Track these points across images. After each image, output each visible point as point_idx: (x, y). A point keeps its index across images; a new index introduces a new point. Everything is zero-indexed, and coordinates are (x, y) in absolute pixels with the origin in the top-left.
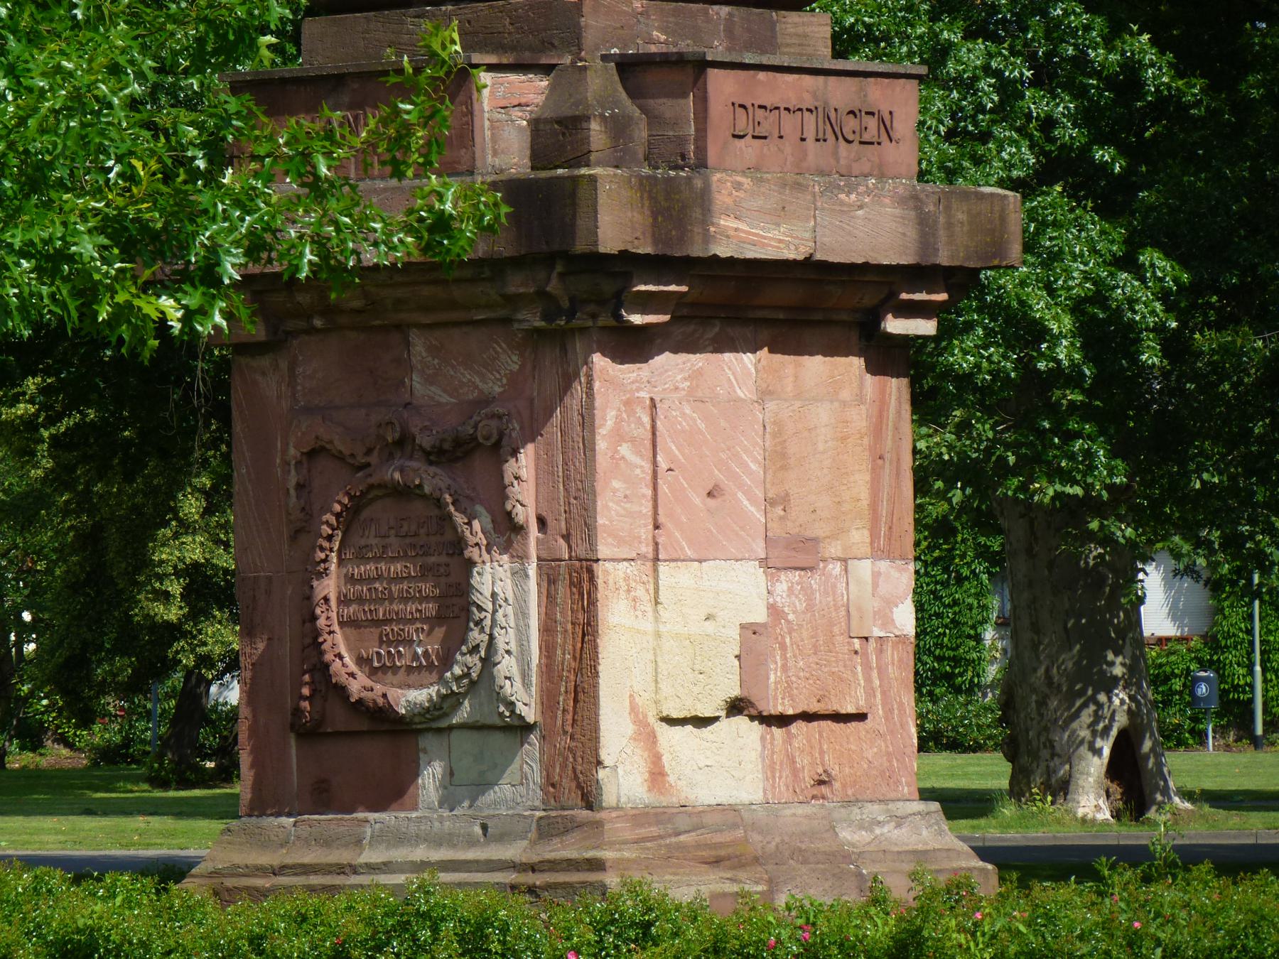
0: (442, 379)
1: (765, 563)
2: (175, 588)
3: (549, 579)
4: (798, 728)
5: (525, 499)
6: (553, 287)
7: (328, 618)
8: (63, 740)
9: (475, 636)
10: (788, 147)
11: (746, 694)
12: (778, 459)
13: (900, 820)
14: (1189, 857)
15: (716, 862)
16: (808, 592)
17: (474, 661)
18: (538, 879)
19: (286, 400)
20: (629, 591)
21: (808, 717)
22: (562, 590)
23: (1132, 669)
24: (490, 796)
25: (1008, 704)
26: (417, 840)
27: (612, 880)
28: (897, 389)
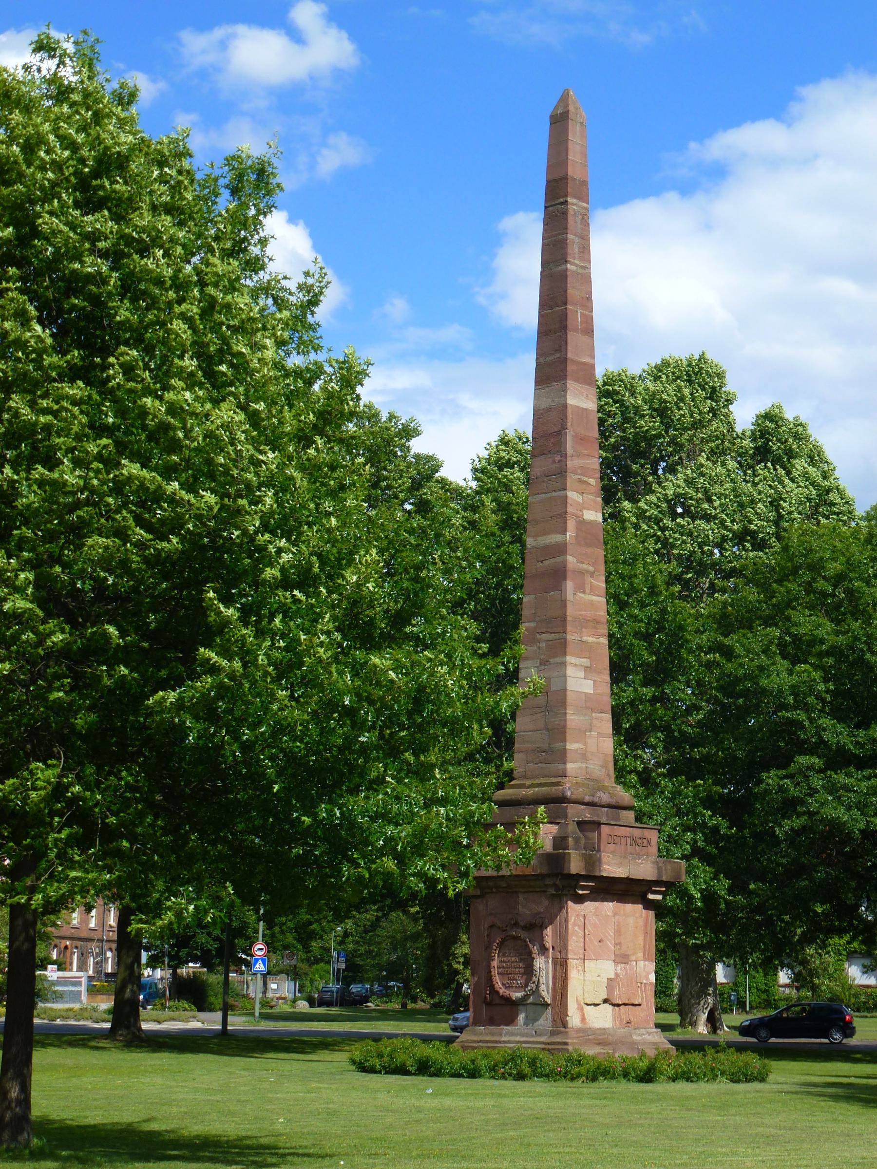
0: (527, 907)
1: (614, 961)
2: (462, 960)
3: (555, 963)
4: (622, 1007)
5: (549, 941)
6: (558, 882)
7: (495, 972)
8: (423, 1001)
9: (534, 979)
10: (623, 846)
12: (618, 932)
13: (649, 1034)
14: (730, 1045)
15: (599, 1044)
16: (626, 969)
17: (534, 986)
18: (550, 1047)
19: (485, 910)
21: (625, 1004)
22: (558, 967)
23: (714, 992)
24: (538, 1023)
25: (680, 1001)
26: (517, 1035)
27: (570, 1048)
28: (651, 914)
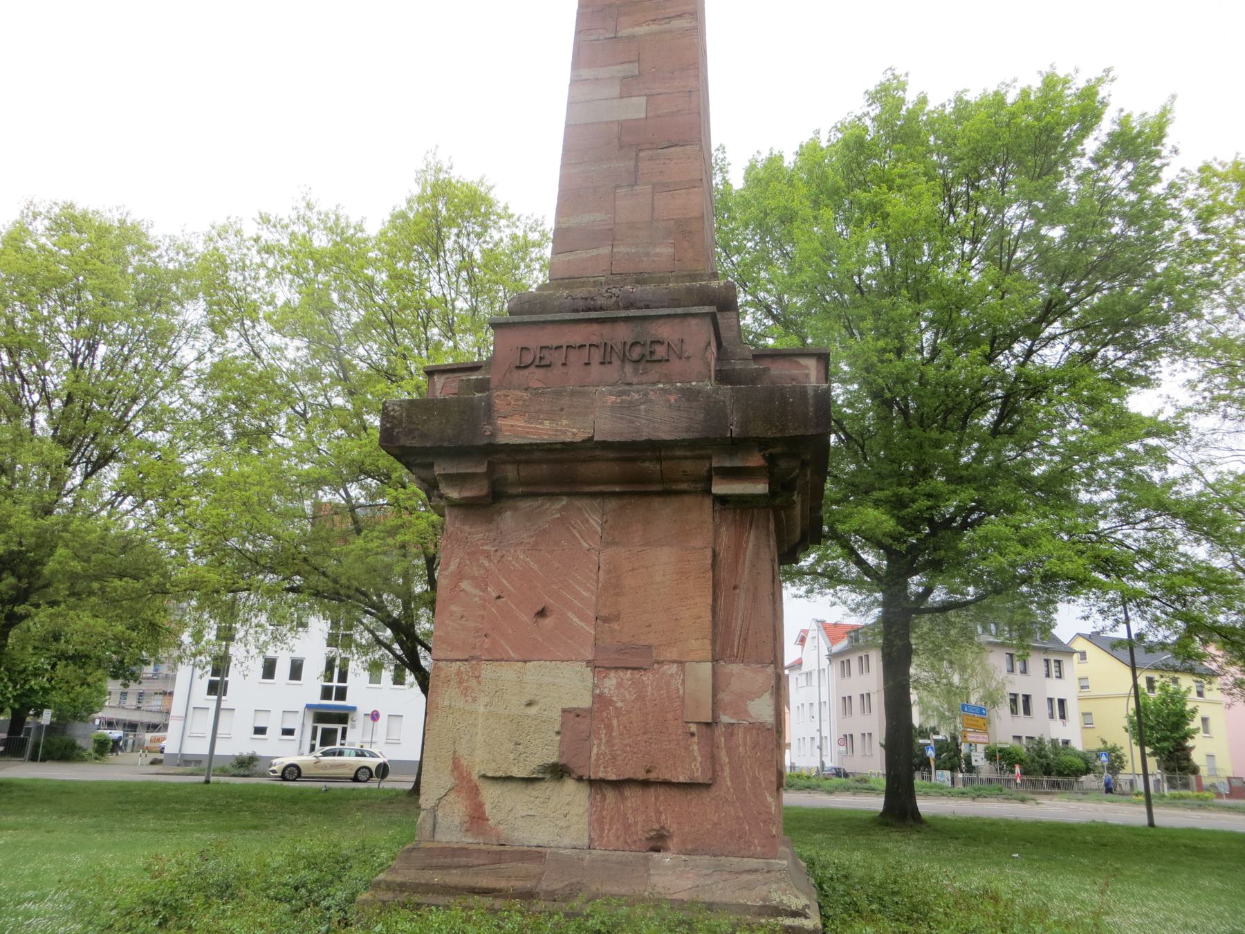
1: (593, 665)
11: (563, 761)
20: (461, 682)
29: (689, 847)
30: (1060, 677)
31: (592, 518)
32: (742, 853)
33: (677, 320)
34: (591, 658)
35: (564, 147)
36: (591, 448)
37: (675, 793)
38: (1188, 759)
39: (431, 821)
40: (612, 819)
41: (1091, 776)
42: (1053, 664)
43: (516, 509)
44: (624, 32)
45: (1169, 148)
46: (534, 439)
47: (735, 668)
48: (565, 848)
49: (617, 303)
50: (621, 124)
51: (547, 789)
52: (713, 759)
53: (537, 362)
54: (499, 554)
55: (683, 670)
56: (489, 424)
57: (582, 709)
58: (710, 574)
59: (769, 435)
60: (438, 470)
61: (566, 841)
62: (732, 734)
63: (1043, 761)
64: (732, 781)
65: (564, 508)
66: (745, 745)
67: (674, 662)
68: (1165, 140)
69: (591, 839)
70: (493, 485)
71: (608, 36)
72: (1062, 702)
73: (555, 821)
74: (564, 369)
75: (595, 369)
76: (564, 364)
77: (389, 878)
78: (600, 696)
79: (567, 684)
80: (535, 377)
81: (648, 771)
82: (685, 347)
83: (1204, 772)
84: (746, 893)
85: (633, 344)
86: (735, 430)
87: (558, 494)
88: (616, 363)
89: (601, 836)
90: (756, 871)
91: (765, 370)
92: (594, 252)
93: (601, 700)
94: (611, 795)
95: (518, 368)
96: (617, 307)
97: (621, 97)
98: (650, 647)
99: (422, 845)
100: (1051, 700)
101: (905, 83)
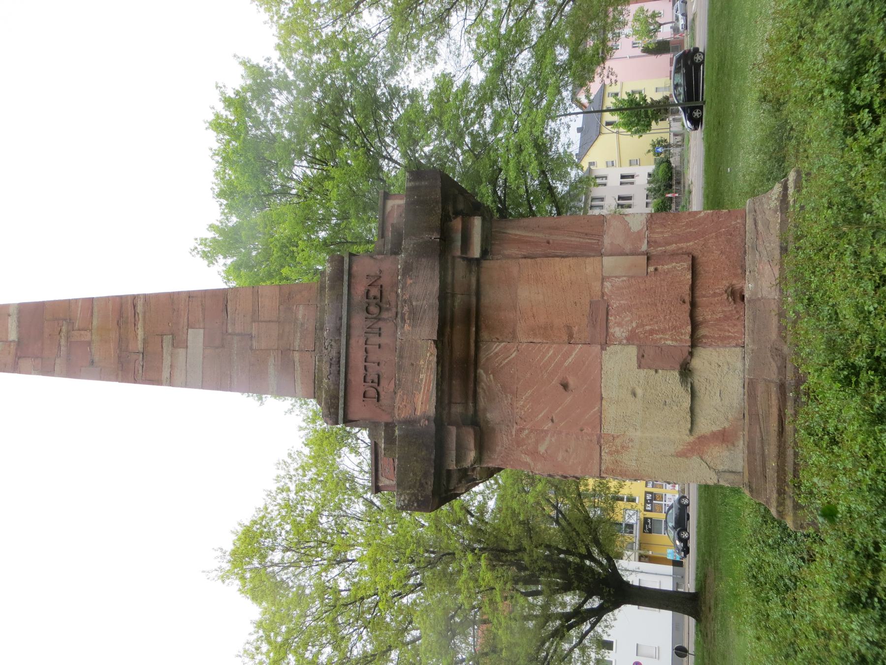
1: (604, 345)
11: (678, 367)
29: (740, 271)
30: (606, 177)
31: (495, 350)
32: (742, 233)
33: (353, 280)
34: (599, 347)
35: (218, 389)
36: (442, 342)
37: (699, 283)
38: (659, 102)
39: (727, 474)
40: (720, 330)
41: (672, 160)
42: (594, 203)
43: (485, 410)
44: (140, 346)
45: (265, 63)
46: (433, 386)
47: (607, 240)
48: (744, 364)
49: (335, 341)
50: (205, 346)
51: (699, 379)
52: (673, 255)
53: (375, 385)
54: (519, 421)
55: (608, 278)
56: (419, 422)
57: (638, 353)
58: (539, 260)
59: (440, 211)
60: (453, 466)
61: (739, 365)
62: (655, 242)
63: (662, 188)
64: (690, 241)
65: (486, 373)
66: (662, 233)
67: (602, 284)
68: (261, 66)
69: (737, 345)
70: (465, 424)
71: (141, 359)
72: (623, 177)
73: (724, 372)
74: (382, 365)
75: (384, 340)
76: (379, 364)
77: (775, 504)
78: (628, 339)
79: (619, 364)
80: (386, 387)
81: (684, 302)
82: (373, 274)
83: (667, 94)
84: (771, 226)
85: (368, 312)
86: (435, 236)
87: (475, 376)
88: (381, 324)
89: (734, 338)
90: (755, 220)
91: (393, 225)
92: (297, 364)
93: (631, 339)
94: (702, 331)
95: (378, 401)
96: (338, 341)
97: (187, 347)
98: (591, 303)
99: (746, 480)
100: (621, 184)
101: (202, 240)
